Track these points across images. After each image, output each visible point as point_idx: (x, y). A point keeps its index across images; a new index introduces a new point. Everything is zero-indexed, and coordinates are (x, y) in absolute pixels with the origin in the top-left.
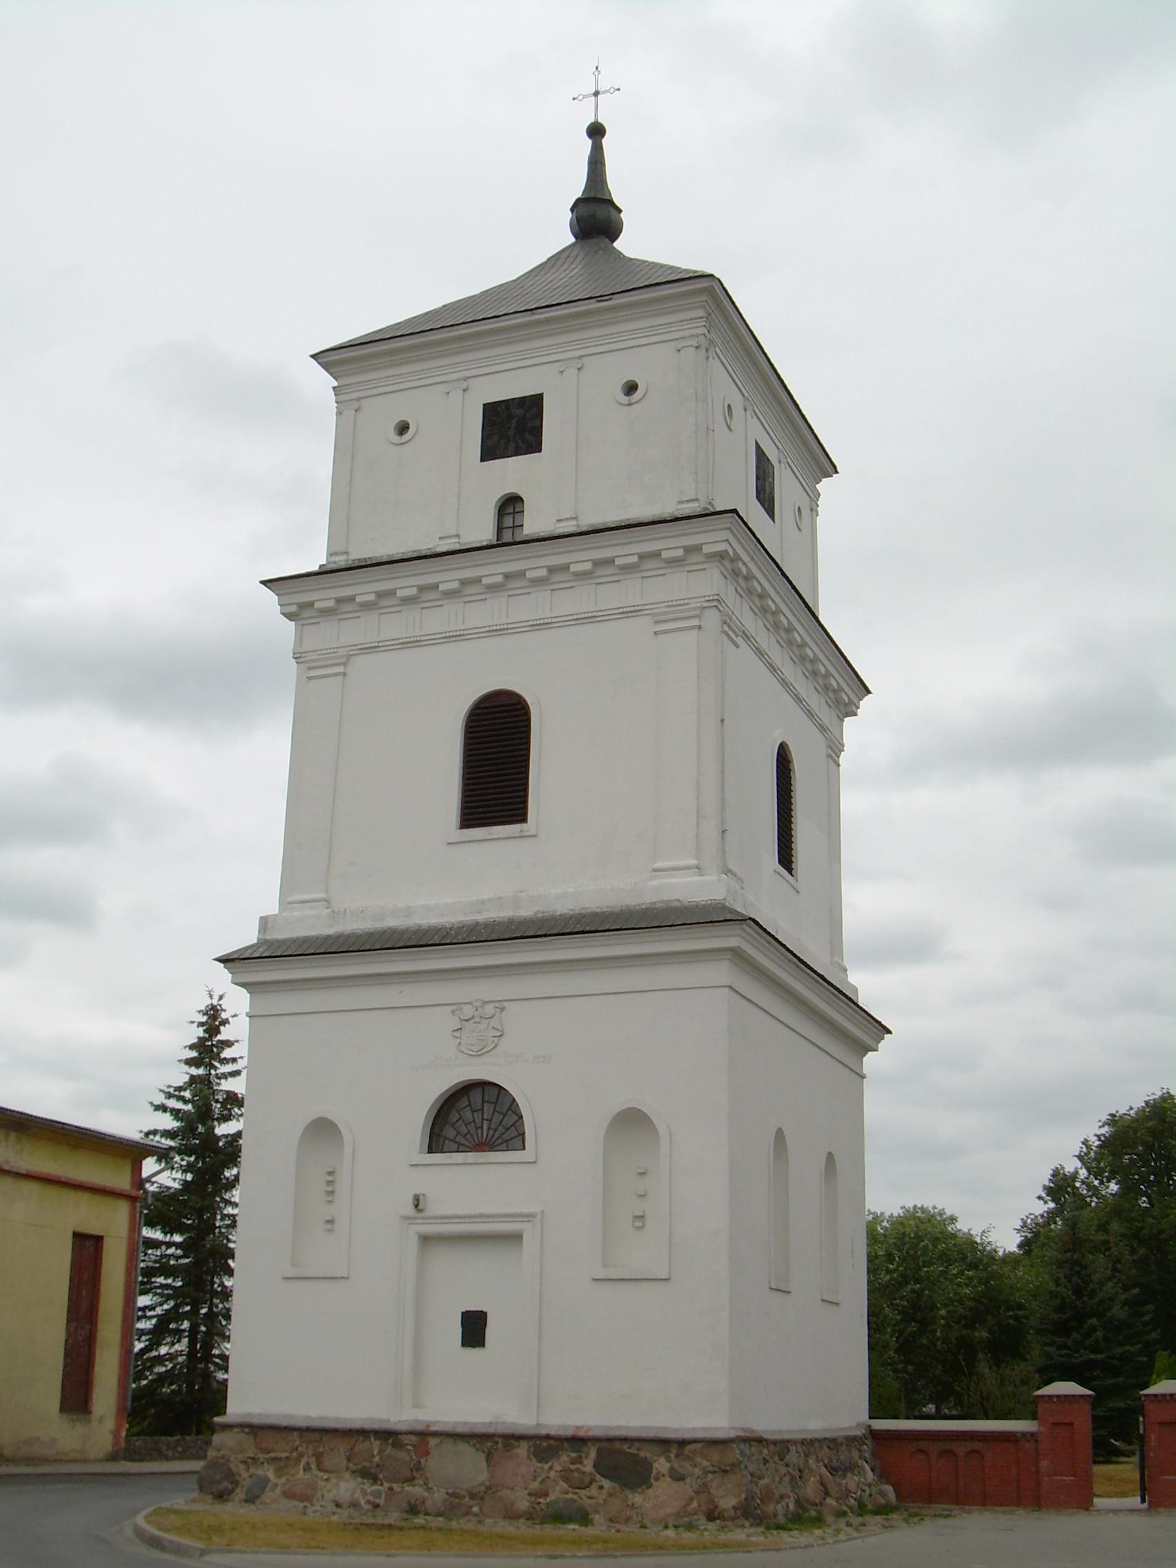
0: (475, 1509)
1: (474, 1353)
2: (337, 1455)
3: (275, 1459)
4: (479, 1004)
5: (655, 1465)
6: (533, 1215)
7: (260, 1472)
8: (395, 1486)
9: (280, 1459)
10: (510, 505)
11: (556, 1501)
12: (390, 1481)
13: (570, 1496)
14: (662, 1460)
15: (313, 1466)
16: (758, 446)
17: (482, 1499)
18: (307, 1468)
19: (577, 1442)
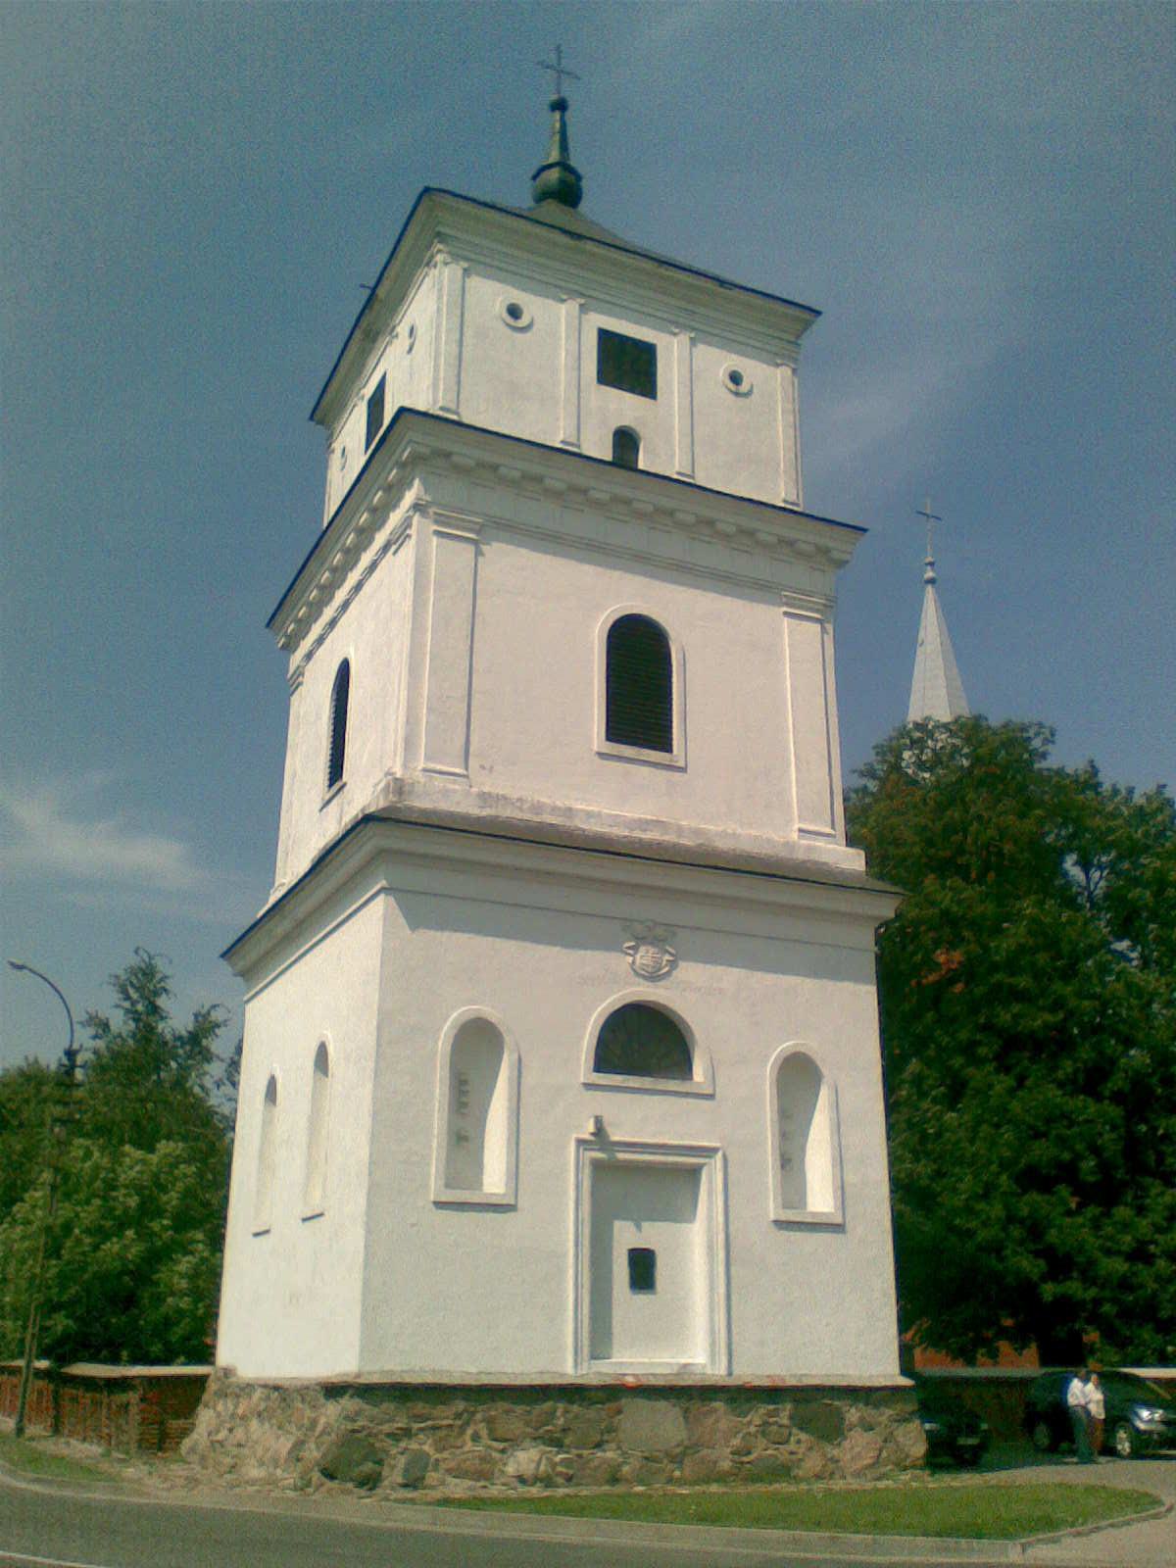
0: (677, 1473)
1: (642, 1298)
2: (514, 1418)
3: (435, 1428)
4: (650, 924)
5: (848, 1416)
6: (715, 1150)
7: (414, 1446)
8: (585, 1452)
9: (439, 1428)
10: (626, 441)
11: (759, 1458)
12: (577, 1448)
13: (769, 1452)
14: (853, 1410)
15: (484, 1433)
16: (384, 378)
17: (681, 1462)
18: (476, 1438)
19: (773, 1393)
